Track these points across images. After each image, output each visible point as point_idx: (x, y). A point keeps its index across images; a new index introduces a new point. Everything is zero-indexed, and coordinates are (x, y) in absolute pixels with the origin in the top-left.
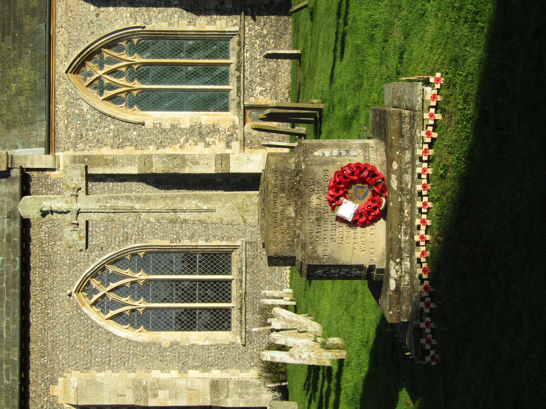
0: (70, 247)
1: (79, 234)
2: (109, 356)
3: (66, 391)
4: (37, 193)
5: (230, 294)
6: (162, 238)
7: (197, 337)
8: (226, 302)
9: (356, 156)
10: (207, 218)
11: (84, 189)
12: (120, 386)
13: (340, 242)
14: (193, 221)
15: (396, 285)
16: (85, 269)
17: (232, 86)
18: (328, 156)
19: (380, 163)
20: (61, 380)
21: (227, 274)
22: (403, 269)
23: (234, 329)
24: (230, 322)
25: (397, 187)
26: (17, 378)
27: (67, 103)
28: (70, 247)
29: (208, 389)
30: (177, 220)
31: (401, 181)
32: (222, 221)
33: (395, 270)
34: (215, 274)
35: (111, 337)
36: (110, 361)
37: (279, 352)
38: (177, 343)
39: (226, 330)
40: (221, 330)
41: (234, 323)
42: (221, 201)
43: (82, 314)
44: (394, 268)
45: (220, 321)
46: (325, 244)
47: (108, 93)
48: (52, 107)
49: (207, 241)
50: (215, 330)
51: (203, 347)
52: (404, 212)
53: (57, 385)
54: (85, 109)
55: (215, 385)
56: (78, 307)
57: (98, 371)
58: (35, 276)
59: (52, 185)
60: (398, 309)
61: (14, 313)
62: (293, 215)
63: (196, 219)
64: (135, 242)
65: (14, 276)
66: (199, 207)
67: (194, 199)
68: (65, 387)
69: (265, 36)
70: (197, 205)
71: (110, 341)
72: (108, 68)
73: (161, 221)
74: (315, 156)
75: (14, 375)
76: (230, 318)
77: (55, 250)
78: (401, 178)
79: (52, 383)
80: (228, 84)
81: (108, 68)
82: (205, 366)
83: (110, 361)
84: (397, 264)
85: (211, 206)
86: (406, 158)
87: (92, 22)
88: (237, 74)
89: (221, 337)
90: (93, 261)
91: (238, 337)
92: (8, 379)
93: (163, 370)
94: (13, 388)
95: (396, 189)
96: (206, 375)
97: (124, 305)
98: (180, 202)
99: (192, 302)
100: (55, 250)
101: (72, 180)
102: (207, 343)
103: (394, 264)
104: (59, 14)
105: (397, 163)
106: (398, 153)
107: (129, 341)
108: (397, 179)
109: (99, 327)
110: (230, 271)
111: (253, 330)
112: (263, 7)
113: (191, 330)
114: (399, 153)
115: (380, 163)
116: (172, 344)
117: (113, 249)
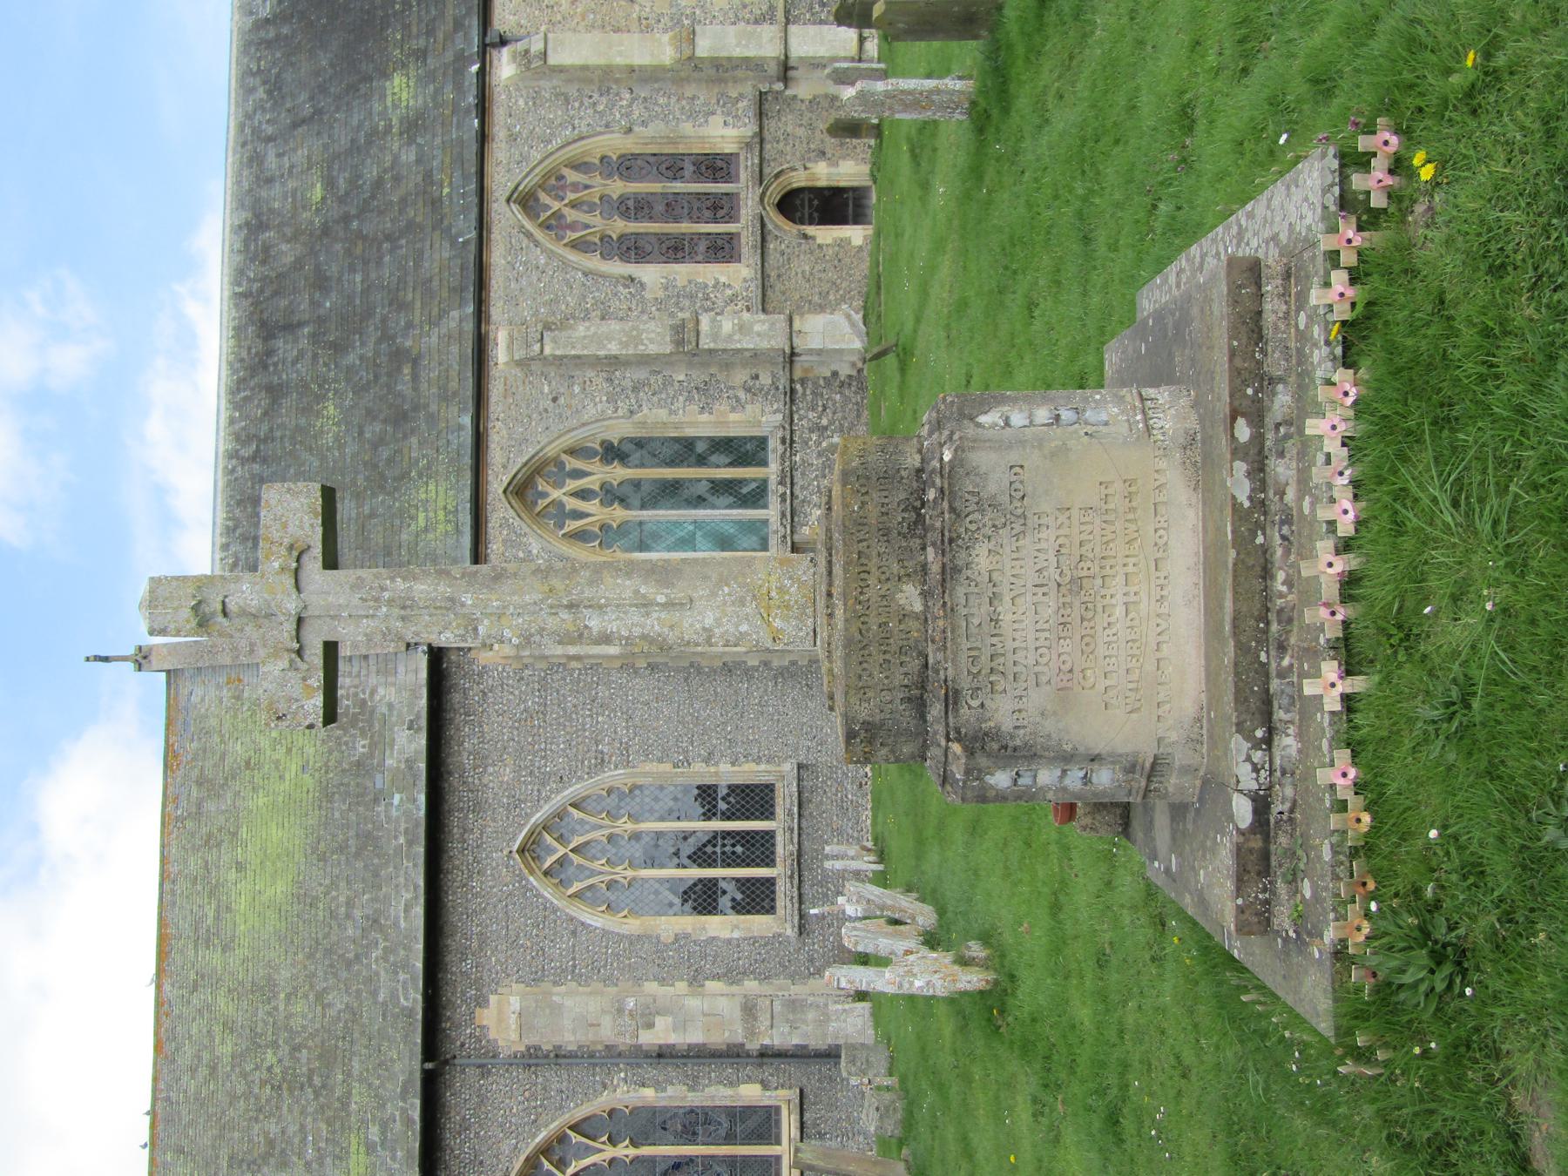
0: (279, 718)
1: (304, 679)
2: (574, 959)
3: (501, 1019)
4: (686, 790)
5: (773, 853)
6: (660, 761)
7: (722, 926)
8: (767, 865)
9: (1106, 424)
10: (666, 630)
11: (317, 550)
12: (591, 1009)
13: (1061, 685)
14: (627, 638)
15: (1256, 812)
16: (532, 814)
17: (772, 471)
18: (1021, 423)
19: (1182, 440)
20: (493, 999)
21: (767, 818)
22: (1277, 762)
23: (780, 911)
24: (773, 900)
25: (1250, 498)
26: (420, 998)
27: (505, 542)
28: (279, 718)
29: (738, 1013)
30: (581, 635)
31: (1263, 481)
32: (710, 637)
33: (1249, 767)
34: (748, 818)
35: (577, 928)
36: (574, 966)
37: (861, 968)
38: (687, 936)
39: (768, 912)
40: (758, 912)
41: (781, 902)
42: (706, 578)
43: (528, 888)
44: (1248, 759)
45: (757, 898)
46: (1017, 693)
47: (572, 525)
48: (482, 548)
49: (733, 764)
50: (749, 912)
51: (729, 941)
52: (1273, 577)
53: (487, 1007)
54: (535, 552)
55: (749, 1010)
56: (522, 878)
57: (555, 983)
58: (455, 823)
59: (480, 675)
60: (1265, 890)
61: (416, 887)
62: (918, 607)
63: (637, 631)
64: (616, 767)
65: (417, 826)
66: (644, 596)
67: (629, 575)
68: (500, 1012)
69: (826, 428)
70: (637, 592)
71: (574, 933)
72: (572, 485)
73: (537, 638)
74: (979, 425)
75: (416, 990)
76: (773, 892)
77: (485, 781)
78: (1262, 470)
79: (479, 1005)
80: (765, 507)
81: (572, 485)
82: (731, 975)
83: (574, 966)
84: (1256, 745)
85: (678, 594)
86: (1276, 406)
87: (546, 410)
88: (781, 489)
89: (759, 924)
90: (548, 799)
91: (788, 926)
92: (406, 999)
93: (662, 981)
94: (411, 1011)
95: (1247, 504)
96: (734, 989)
97: (593, 873)
98: (591, 583)
99: (710, 866)
100: (485, 781)
101: (285, 526)
102: (736, 935)
103: (1246, 745)
104: (493, 400)
105: (1250, 423)
106: (1250, 391)
107: (605, 933)
108: (1249, 474)
109: (555, 910)
110: (773, 813)
111: (812, 911)
112: (822, 382)
113: (710, 913)
114: (1256, 392)
115: (1182, 440)
116: (677, 938)
117: (580, 778)
